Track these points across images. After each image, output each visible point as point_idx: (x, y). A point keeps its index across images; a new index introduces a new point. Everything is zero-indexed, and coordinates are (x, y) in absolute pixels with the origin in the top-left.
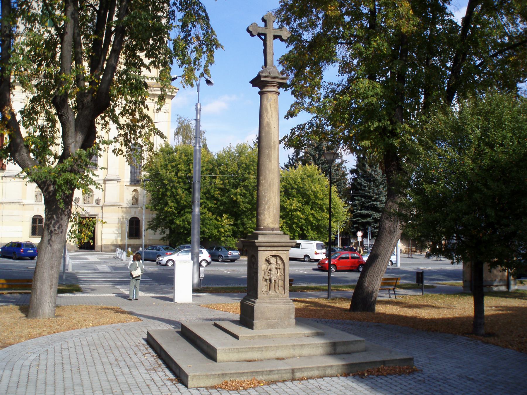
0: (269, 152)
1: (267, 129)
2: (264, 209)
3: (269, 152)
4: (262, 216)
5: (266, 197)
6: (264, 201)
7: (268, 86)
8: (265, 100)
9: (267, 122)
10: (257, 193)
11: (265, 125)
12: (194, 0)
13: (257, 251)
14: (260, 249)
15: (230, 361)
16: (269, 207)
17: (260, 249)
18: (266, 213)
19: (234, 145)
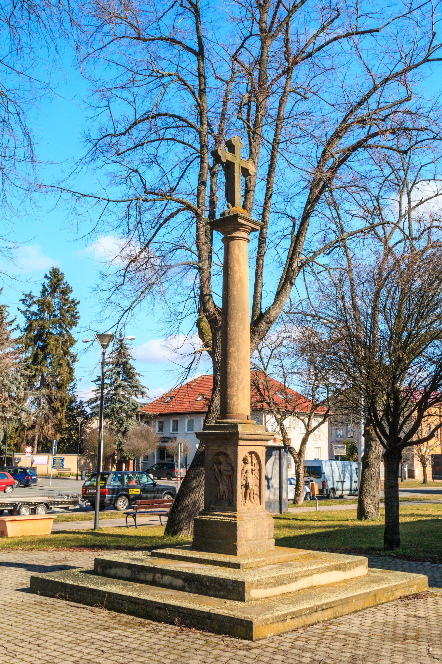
0: (242, 316)
1: (239, 286)
2: (237, 390)
3: (242, 316)
4: (235, 399)
5: (239, 374)
6: (238, 379)
7: (239, 230)
8: (237, 248)
9: (240, 277)
10: (272, 597)
11: (236, 280)
12: (1, 409)
13: (237, 445)
14: (240, 442)
15: (232, 485)
16: (243, 388)
17: (240, 442)
18: (240, 395)
19: (325, 471)
